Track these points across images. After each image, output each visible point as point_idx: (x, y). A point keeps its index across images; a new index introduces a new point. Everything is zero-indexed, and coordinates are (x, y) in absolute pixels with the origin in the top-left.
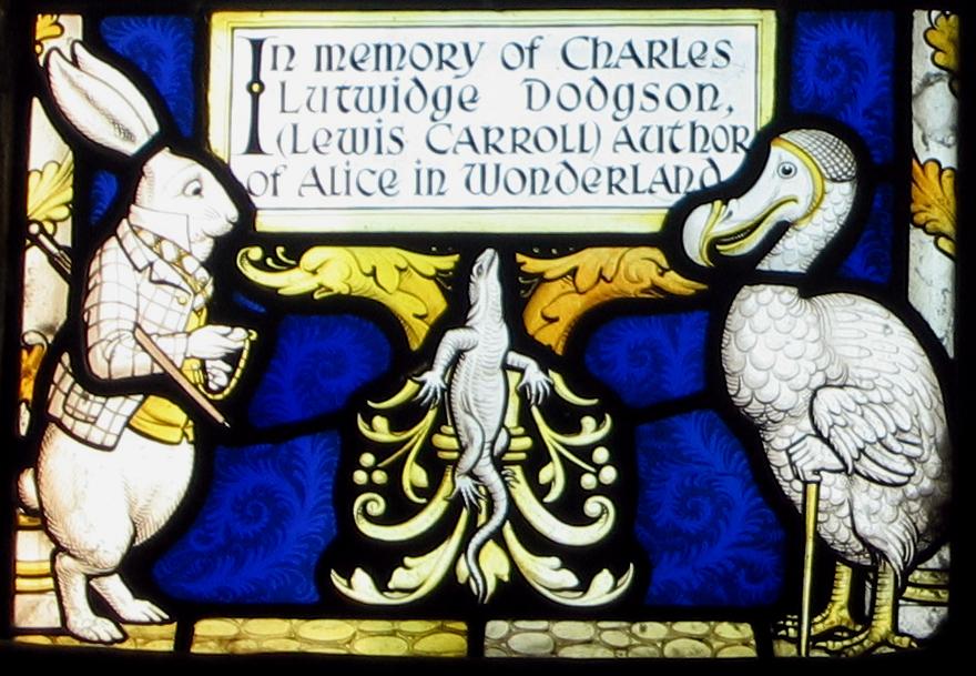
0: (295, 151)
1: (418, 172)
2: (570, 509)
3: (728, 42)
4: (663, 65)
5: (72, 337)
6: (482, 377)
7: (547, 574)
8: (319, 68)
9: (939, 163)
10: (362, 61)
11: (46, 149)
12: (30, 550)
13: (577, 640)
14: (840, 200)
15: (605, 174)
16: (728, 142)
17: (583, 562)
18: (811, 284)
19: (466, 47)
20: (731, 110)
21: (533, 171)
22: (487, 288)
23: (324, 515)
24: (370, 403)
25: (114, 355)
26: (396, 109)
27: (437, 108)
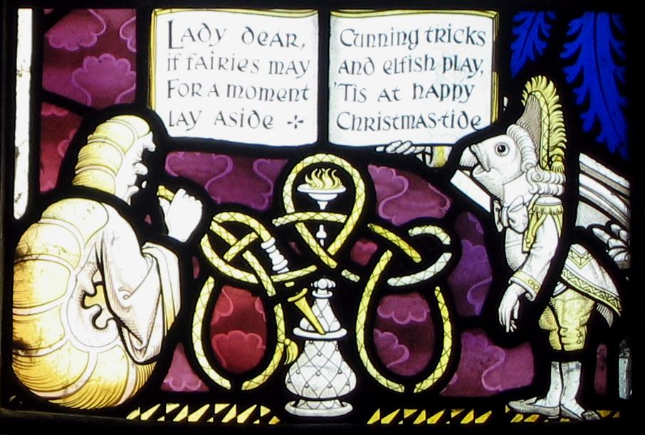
3: (434, 114)
8: (228, 96)
9: (92, 296)
10: (389, 69)
15: (363, 121)
20: (84, 219)
26: (261, 98)
27: (411, 43)
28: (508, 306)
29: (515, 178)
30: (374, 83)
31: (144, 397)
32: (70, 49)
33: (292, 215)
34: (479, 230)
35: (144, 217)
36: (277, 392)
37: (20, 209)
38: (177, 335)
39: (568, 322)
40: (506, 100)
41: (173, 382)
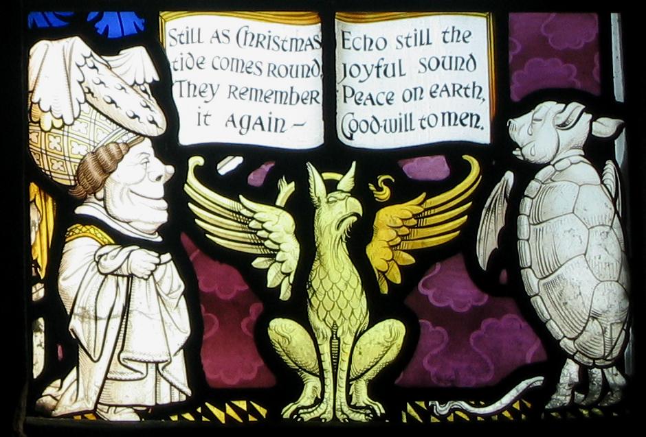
0: (199, 42)
1: (270, 119)
3: (261, 63)
4: (460, 95)
8: (411, 115)
16: (228, 66)
19: (211, 85)
21: (233, 59)
23: (388, 220)
24: (393, 180)
26: (443, 125)
32: (538, 59)
37: (38, 369)
40: (74, 337)
41: (553, 38)
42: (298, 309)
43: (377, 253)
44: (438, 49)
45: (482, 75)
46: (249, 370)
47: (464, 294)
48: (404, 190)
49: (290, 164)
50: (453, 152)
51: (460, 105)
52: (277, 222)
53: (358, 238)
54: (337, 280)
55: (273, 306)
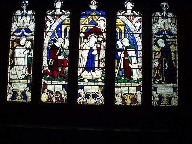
2: (21, 97)
5: (9, 92)
6: (19, 94)
7: (21, 99)
11: (8, 87)
12: (7, 98)
13: (22, 101)
14: (29, 89)
17: (22, 99)
18: (28, 91)
22: (19, 91)
25: (10, 93)
28: (62, 98)
29: (62, 92)
30: (57, 88)
31: (47, 101)
33: (53, 94)
34: (61, 95)
35: (47, 94)
36: (52, 101)
37: (42, 93)
38: (48, 99)
39: (65, 99)
42: (127, 100)
43: (130, 98)
44: (133, 89)
45: (135, 90)
46: (125, 103)
47: (134, 100)
48: (132, 95)
49: (127, 94)
50: (134, 93)
51: (134, 91)
52: (126, 96)
53: (129, 97)
54: (128, 99)
55: (126, 100)
